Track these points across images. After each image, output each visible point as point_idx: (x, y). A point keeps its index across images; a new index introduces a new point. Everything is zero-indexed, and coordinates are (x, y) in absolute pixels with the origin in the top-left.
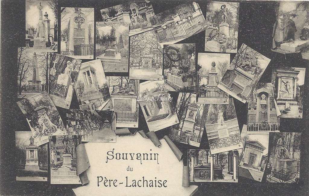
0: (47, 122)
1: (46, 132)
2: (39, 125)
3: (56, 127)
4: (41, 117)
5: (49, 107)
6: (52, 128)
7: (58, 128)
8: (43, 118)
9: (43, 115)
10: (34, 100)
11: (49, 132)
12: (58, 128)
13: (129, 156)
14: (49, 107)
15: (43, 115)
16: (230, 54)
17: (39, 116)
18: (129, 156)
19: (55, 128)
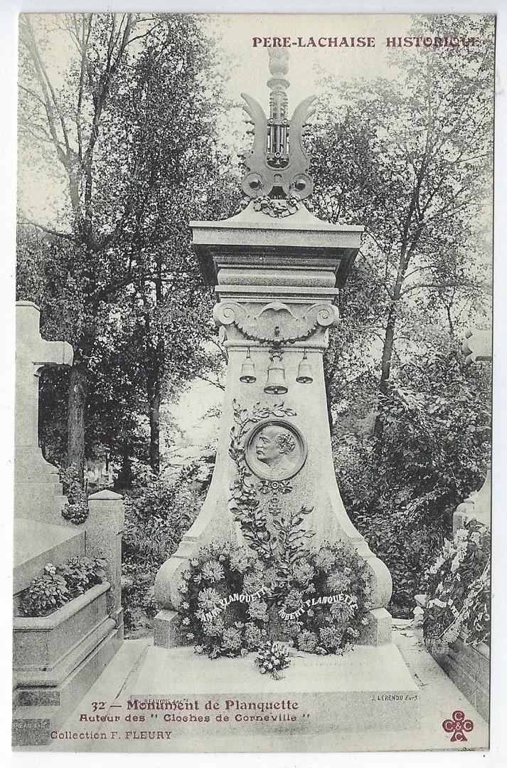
0: (288, 465)
1: (210, 598)
2: (153, 457)
3: (381, 577)
4: (237, 363)
5: (418, 270)
6: (320, 578)
7: (400, 604)
8: (251, 398)
9: (276, 347)
10: (277, 84)
11: (258, 610)
12: (400, 604)
13: (349, 43)
14: (418, 270)
15: (276, 347)
16: (490, 355)
17: (209, 348)
18: (349, 43)
19: (358, 588)
